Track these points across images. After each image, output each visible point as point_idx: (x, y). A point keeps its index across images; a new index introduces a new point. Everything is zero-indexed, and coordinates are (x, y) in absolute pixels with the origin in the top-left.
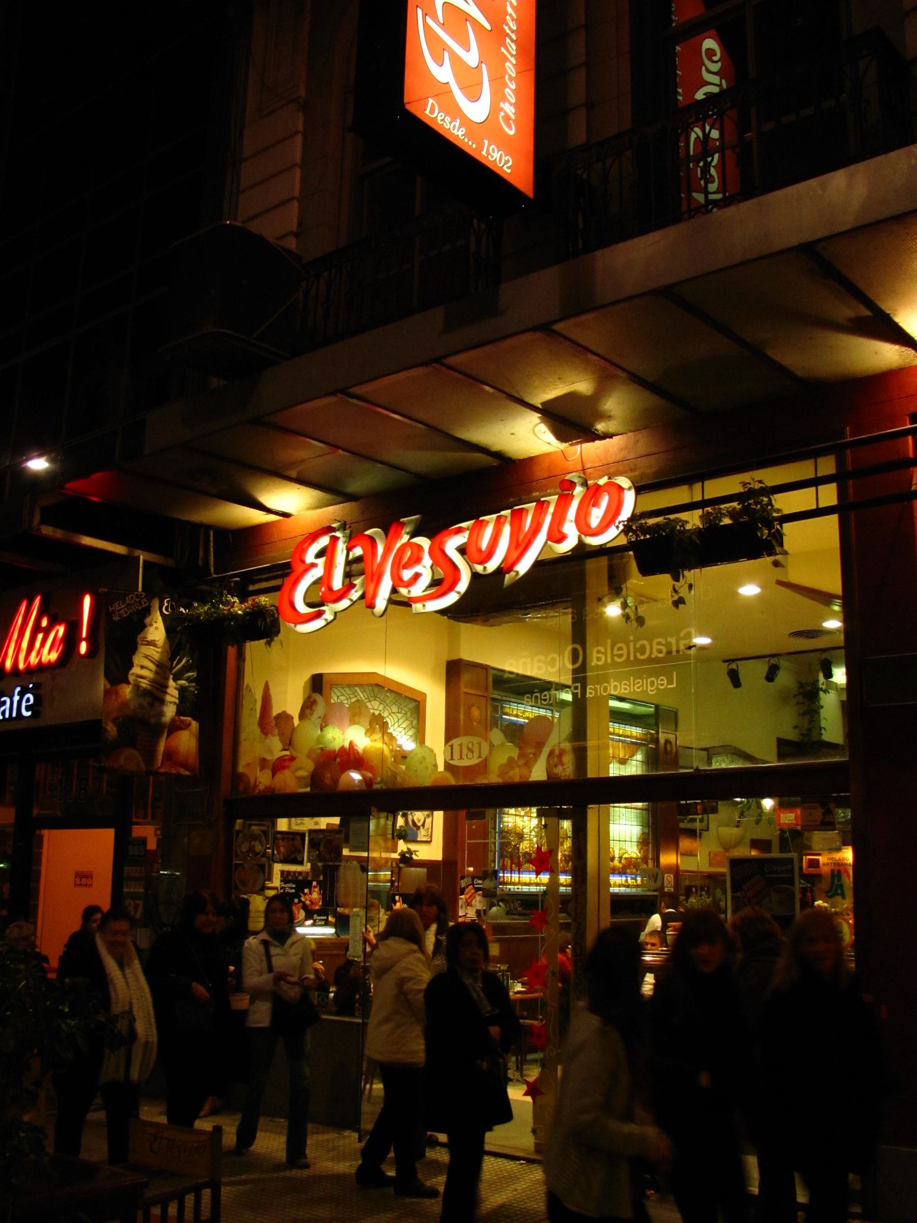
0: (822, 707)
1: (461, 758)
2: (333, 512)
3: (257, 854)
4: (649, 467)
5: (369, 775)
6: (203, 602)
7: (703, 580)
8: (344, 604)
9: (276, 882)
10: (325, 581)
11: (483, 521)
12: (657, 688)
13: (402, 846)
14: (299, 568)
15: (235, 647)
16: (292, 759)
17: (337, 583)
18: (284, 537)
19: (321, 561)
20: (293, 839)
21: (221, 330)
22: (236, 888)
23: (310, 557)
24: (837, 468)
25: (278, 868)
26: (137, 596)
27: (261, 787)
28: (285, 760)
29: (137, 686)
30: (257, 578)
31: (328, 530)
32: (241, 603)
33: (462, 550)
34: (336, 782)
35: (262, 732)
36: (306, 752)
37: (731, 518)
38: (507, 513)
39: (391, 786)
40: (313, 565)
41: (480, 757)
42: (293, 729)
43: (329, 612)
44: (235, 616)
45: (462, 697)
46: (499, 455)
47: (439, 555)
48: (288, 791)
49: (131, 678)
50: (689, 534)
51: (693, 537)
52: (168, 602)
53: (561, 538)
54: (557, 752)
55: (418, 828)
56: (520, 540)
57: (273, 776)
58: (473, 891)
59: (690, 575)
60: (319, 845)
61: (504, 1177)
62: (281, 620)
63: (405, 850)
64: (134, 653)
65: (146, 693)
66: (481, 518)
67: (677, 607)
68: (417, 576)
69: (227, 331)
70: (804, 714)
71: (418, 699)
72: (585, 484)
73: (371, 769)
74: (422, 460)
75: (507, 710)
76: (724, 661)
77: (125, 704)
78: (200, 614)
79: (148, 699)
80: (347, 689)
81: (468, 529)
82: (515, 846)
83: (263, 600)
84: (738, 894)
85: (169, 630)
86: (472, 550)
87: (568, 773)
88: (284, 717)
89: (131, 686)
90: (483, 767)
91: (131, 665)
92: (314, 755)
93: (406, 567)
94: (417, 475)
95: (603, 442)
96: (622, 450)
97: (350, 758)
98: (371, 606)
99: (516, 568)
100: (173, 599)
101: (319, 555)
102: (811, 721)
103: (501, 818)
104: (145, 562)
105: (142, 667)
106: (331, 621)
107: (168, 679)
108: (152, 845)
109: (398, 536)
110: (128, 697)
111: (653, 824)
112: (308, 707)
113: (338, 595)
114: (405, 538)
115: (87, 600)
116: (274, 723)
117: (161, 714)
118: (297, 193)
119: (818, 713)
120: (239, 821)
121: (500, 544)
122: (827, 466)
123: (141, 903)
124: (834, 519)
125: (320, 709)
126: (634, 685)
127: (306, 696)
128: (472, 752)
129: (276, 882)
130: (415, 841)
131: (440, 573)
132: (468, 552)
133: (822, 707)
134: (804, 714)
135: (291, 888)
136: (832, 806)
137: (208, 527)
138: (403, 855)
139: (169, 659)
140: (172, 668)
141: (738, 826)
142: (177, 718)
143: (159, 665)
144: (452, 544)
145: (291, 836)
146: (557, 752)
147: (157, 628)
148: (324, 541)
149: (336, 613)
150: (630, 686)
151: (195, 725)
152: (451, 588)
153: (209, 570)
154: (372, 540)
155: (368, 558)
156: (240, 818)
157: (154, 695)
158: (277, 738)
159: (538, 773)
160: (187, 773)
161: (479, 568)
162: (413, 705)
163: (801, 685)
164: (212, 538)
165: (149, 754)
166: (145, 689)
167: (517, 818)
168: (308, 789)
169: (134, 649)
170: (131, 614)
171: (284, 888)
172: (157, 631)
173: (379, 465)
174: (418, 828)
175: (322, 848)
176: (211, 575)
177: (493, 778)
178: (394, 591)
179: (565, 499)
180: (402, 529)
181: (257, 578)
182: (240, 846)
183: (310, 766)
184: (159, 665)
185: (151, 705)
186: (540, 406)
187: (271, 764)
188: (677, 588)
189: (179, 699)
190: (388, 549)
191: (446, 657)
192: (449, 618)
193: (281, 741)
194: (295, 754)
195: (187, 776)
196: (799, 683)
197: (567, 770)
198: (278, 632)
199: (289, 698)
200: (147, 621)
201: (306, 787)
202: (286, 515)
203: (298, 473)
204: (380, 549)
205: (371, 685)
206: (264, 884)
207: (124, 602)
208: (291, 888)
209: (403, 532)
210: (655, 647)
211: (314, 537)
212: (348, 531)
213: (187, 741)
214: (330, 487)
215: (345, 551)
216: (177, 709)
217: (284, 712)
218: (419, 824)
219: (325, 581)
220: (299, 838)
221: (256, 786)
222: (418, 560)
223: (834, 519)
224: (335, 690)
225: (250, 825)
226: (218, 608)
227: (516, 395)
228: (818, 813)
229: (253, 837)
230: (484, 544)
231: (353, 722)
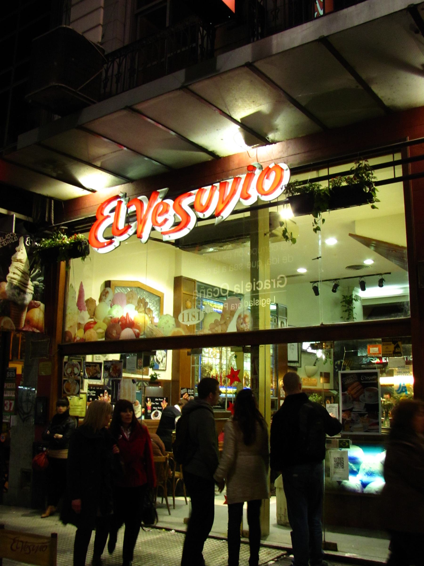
0: (354, 308)
1: (188, 320)
2: (120, 189)
3: (75, 374)
4: (296, 161)
5: (137, 331)
6: (47, 238)
7: (333, 217)
8: (125, 237)
9: (86, 389)
10: (117, 210)
11: (203, 189)
12: (266, 304)
13: (151, 372)
14: (100, 218)
15: (65, 261)
16: (95, 323)
17: (121, 225)
18: (92, 205)
19: (113, 215)
20: (95, 366)
21: (60, 84)
22: (64, 393)
23: (106, 212)
24: (402, 157)
25: (87, 382)
26: (12, 235)
27: (78, 339)
28: (91, 324)
29: (11, 284)
30: (76, 227)
31: (117, 197)
32: (68, 238)
33: (192, 206)
34: (119, 334)
35: (78, 309)
36: (103, 319)
37: (347, 182)
38: (218, 185)
39: (149, 337)
40: (108, 217)
41: (199, 320)
42: (96, 307)
43: (117, 240)
44: (65, 245)
45: (182, 294)
46: (212, 154)
47: (179, 208)
48: (93, 340)
49: (8, 279)
50: (323, 191)
51: (326, 192)
52: (28, 239)
53: (247, 197)
54: (242, 316)
55: (159, 363)
56: (224, 199)
57: (84, 332)
58: (188, 396)
59: (324, 215)
60: (110, 369)
61: (215, 550)
62: (90, 246)
63: (153, 373)
64: (10, 266)
65: (16, 287)
66: (202, 188)
67: (316, 232)
68: (166, 220)
69: (63, 85)
70: (346, 311)
71: (160, 296)
72: (261, 168)
73: (138, 328)
74: (170, 155)
75: (205, 303)
76: (311, 282)
77: (4, 293)
78: (46, 244)
79: (17, 291)
80: (123, 289)
81: (195, 194)
82: (208, 373)
83: (81, 236)
84: (346, 392)
85: (29, 254)
86: (197, 206)
87: (248, 328)
88: (91, 301)
89: (8, 283)
90: (199, 326)
91: (8, 272)
92: (107, 321)
93: (159, 215)
94: (166, 166)
95: (271, 146)
96: (280, 152)
97: (127, 323)
98: (140, 237)
99: (222, 214)
100: (31, 238)
101: (112, 211)
102: (349, 315)
103: (201, 359)
104: (16, 218)
105: (14, 273)
106: (118, 247)
107: (28, 280)
108: (19, 371)
109: (155, 199)
110: (6, 289)
111: (275, 363)
112: (104, 295)
113: (121, 232)
114: (159, 200)
115: (93, 533)
116: (85, 304)
117: (24, 299)
118: (101, 22)
119: (352, 310)
120: (66, 357)
121: (211, 203)
122: (398, 157)
123: (13, 402)
124: (400, 185)
125: (110, 296)
126: (255, 302)
127: (103, 289)
128: (194, 317)
129: (86, 389)
130: (158, 369)
131: (179, 218)
132: (195, 206)
133: (354, 308)
134: (346, 311)
135: (93, 393)
136: (399, 343)
137: (51, 198)
138: (152, 376)
139: (29, 270)
140: (30, 275)
141: (315, 365)
142: (33, 301)
143: (23, 273)
144: (186, 202)
145: (94, 364)
146: (242, 316)
147: (22, 253)
148: (114, 204)
149: (120, 242)
150: (253, 303)
151: (42, 306)
152: (185, 226)
153: (51, 222)
154: (141, 202)
155: (139, 213)
156: (66, 355)
157: (21, 289)
158: (87, 312)
159: (232, 328)
160: (38, 331)
161: (201, 215)
162: (157, 298)
163: (344, 297)
164: (53, 208)
165: (17, 321)
166: (16, 285)
167: (209, 358)
168: (104, 339)
169: (9, 263)
170: (8, 244)
171: (90, 393)
172: (22, 254)
173: (146, 159)
174: (159, 363)
175: (111, 371)
176: (52, 224)
177: (206, 331)
178: (153, 229)
179: (250, 175)
180: (158, 195)
181: (76, 227)
182: (66, 370)
183: (105, 327)
184: (23, 273)
185: (19, 294)
186: (240, 121)
187: (83, 326)
188: (316, 221)
189: (34, 291)
190: (150, 207)
191: (174, 275)
192: (180, 248)
193: (89, 313)
194: (96, 320)
195: (38, 333)
196: (344, 296)
197: (248, 327)
198: (88, 253)
199: (93, 292)
200: (17, 249)
201: (102, 338)
202: (93, 191)
203: (102, 163)
204: (146, 205)
205: (135, 287)
206: (79, 391)
207: (4, 238)
208: (93, 393)
209: (158, 197)
210: (266, 284)
211: (109, 201)
212: (127, 198)
213: (38, 314)
214: (119, 173)
215: (126, 208)
216: (33, 296)
217: (91, 298)
218: (160, 361)
219: (113, 227)
220: (98, 365)
221: (75, 338)
222: (167, 211)
223: (400, 185)
224: (117, 289)
225: (72, 359)
226: (56, 241)
227: (228, 113)
228: (392, 347)
229: (73, 366)
230: (204, 202)
231: (128, 302)
